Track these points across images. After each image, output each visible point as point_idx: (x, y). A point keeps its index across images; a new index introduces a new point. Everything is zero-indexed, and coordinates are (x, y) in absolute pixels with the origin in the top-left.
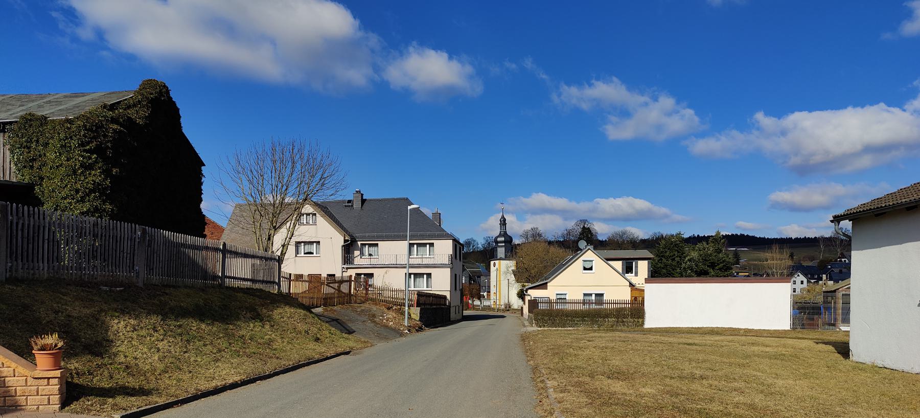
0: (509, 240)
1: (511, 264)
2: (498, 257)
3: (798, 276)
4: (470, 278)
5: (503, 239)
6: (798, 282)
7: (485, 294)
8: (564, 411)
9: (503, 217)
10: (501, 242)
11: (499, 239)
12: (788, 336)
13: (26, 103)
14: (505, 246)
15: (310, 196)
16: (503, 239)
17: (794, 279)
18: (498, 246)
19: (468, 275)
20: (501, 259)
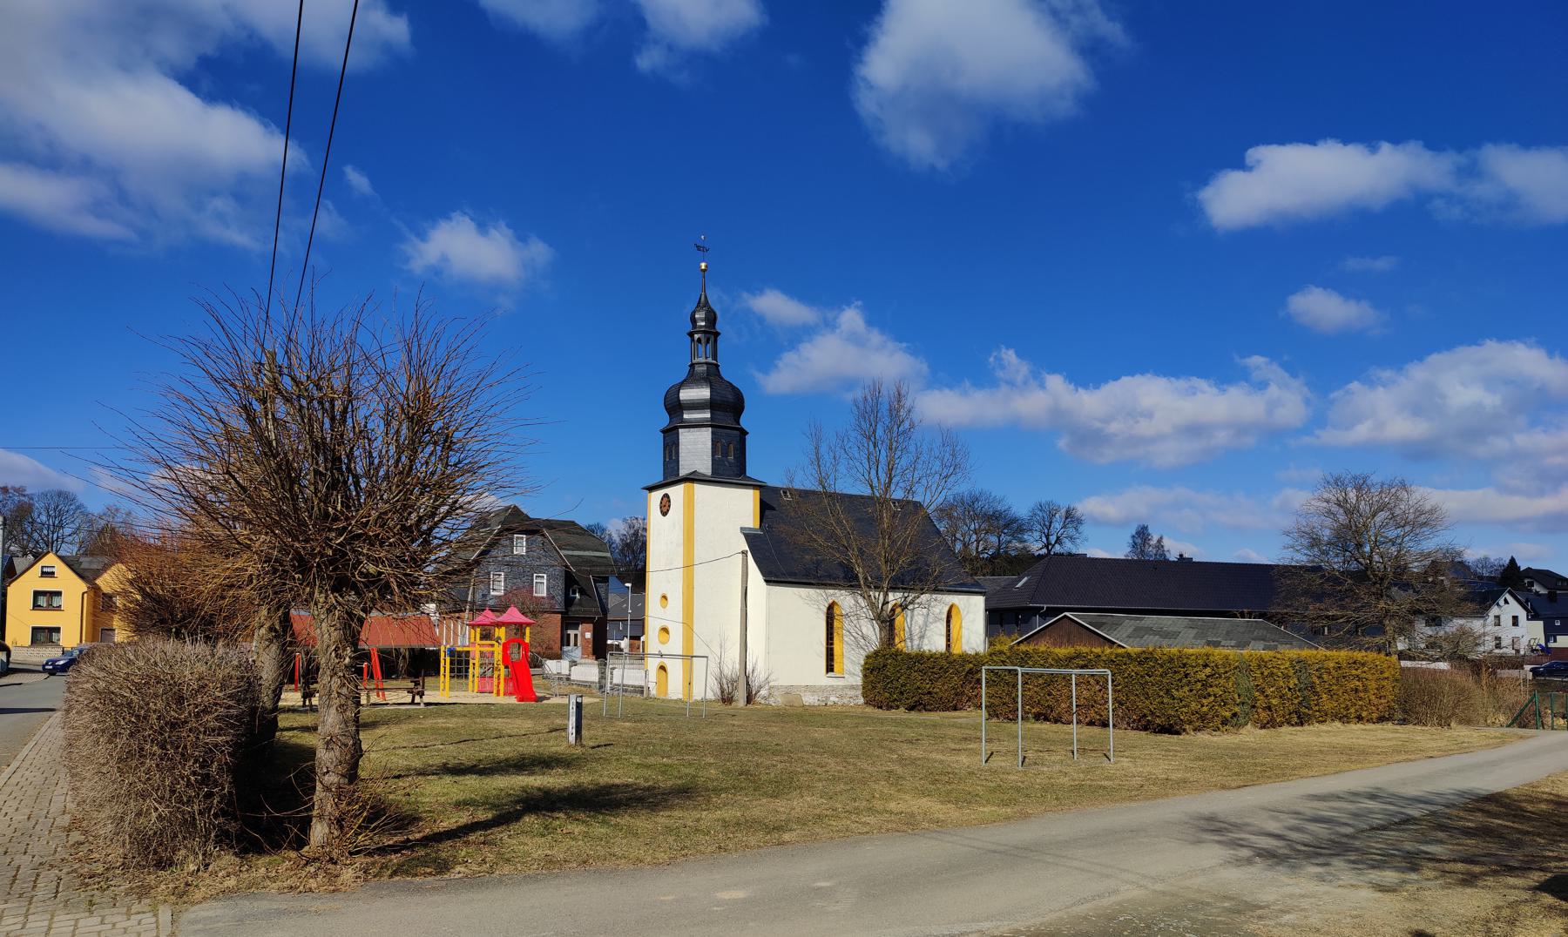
0: (730, 397)
1: (741, 506)
2: (683, 472)
3: (1506, 602)
4: (570, 581)
5: (704, 393)
6: (1506, 620)
7: (624, 644)
8: (1195, 931)
9: (703, 304)
10: (696, 406)
11: (687, 394)
12: (1095, 861)
13: (1344, 818)
14: (713, 425)
15: (384, 451)
16: (704, 393)
17: (1494, 611)
18: (682, 420)
19: (559, 571)
20: (693, 478)
